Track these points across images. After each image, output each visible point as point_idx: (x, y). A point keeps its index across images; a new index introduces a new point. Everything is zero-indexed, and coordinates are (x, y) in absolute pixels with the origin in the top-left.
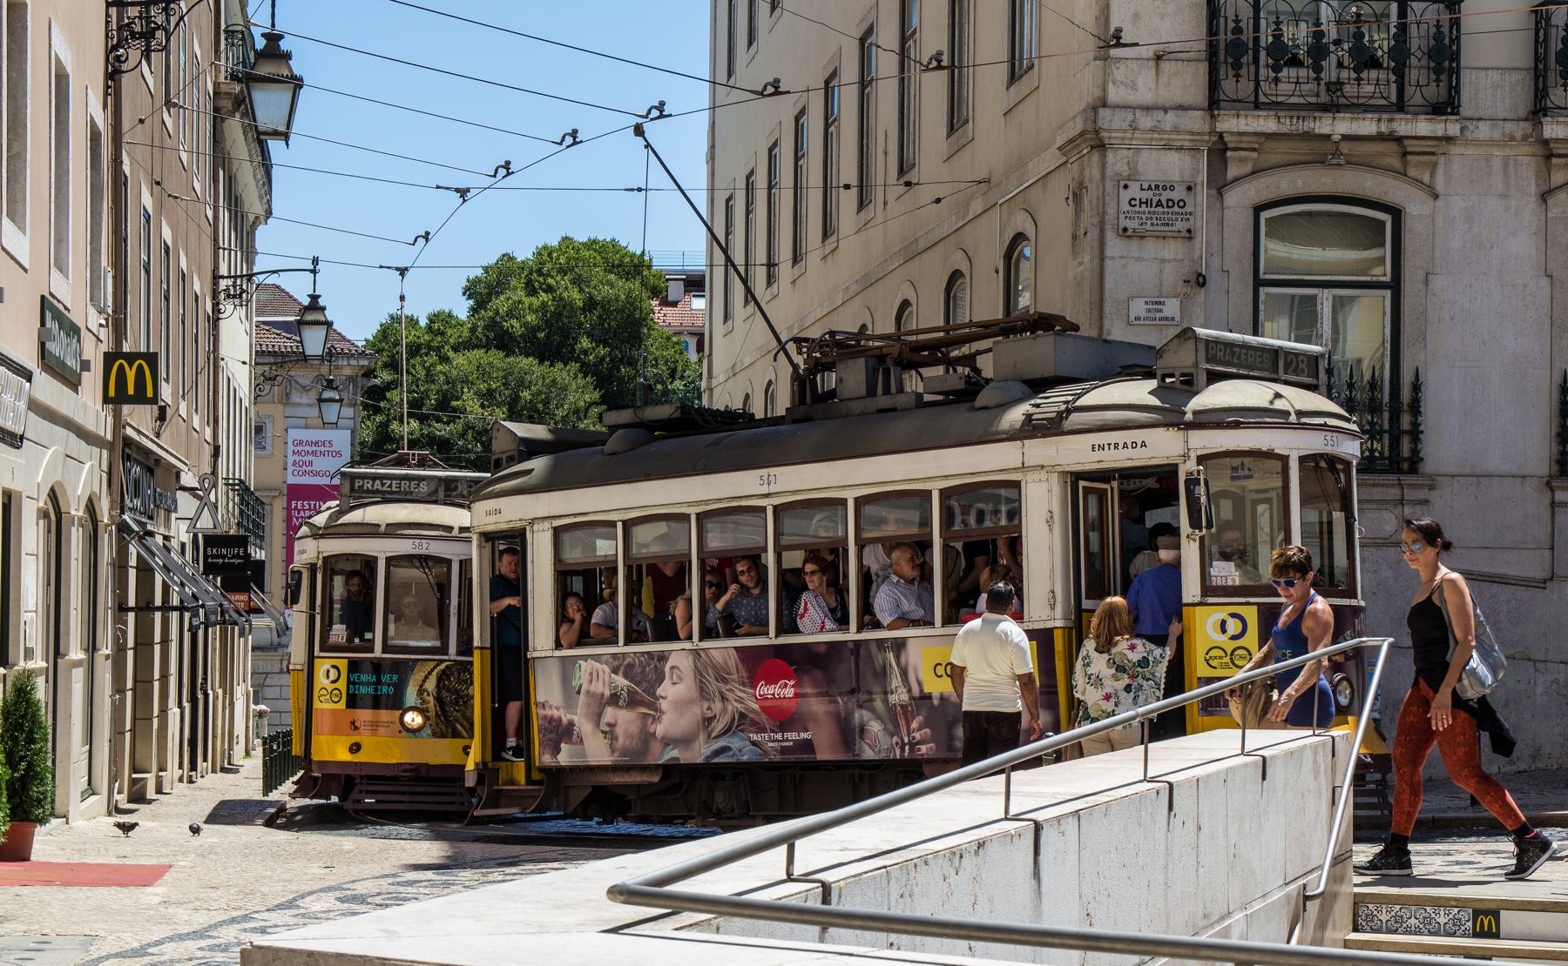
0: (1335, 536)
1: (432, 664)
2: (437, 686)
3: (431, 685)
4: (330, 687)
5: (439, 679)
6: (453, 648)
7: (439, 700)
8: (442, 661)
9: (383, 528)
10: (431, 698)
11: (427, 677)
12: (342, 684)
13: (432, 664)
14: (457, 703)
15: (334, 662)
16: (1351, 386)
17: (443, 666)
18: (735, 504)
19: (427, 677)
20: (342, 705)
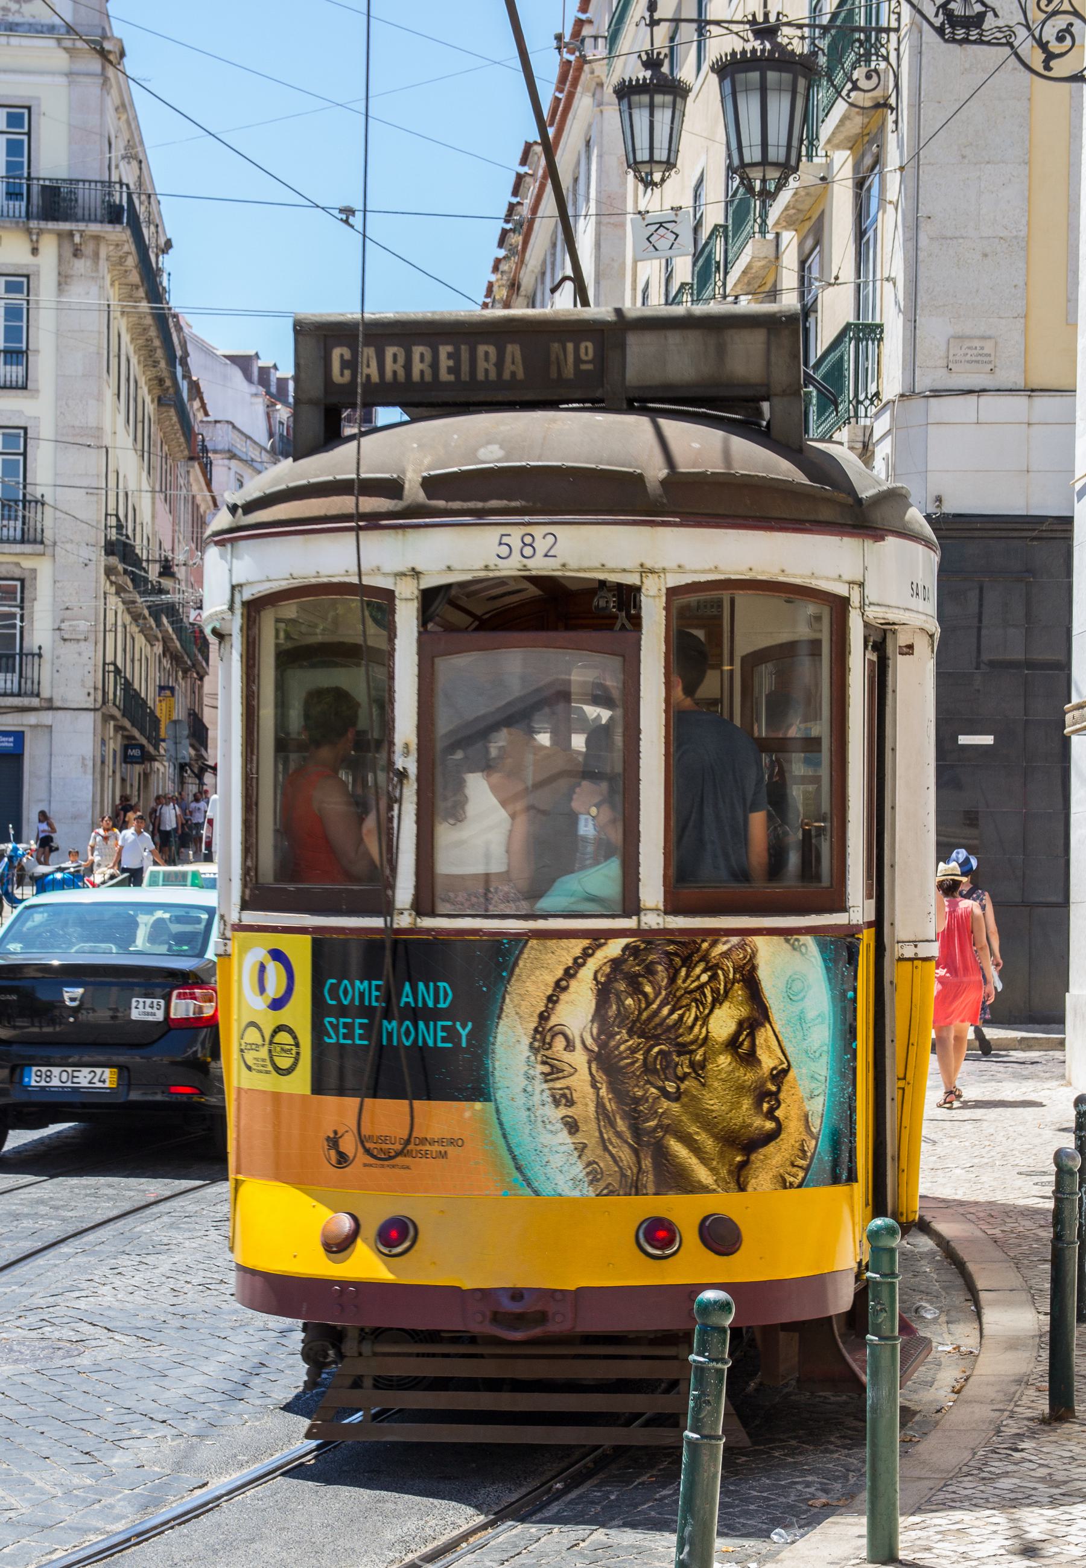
0: (605, 920)
1: (577, 946)
2: (600, 1013)
3: (577, 1012)
4: (270, 1021)
5: (604, 993)
6: (652, 889)
7: (604, 1059)
8: (599, 937)
9: (414, 492)
10: (579, 1059)
11: (560, 987)
12: (299, 1013)
13: (577, 946)
14: (668, 1068)
15: (283, 942)
16: (96, 255)
17: (614, 948)
18: (527, 519)
19: (560, 987)
20: (300, 1082)
